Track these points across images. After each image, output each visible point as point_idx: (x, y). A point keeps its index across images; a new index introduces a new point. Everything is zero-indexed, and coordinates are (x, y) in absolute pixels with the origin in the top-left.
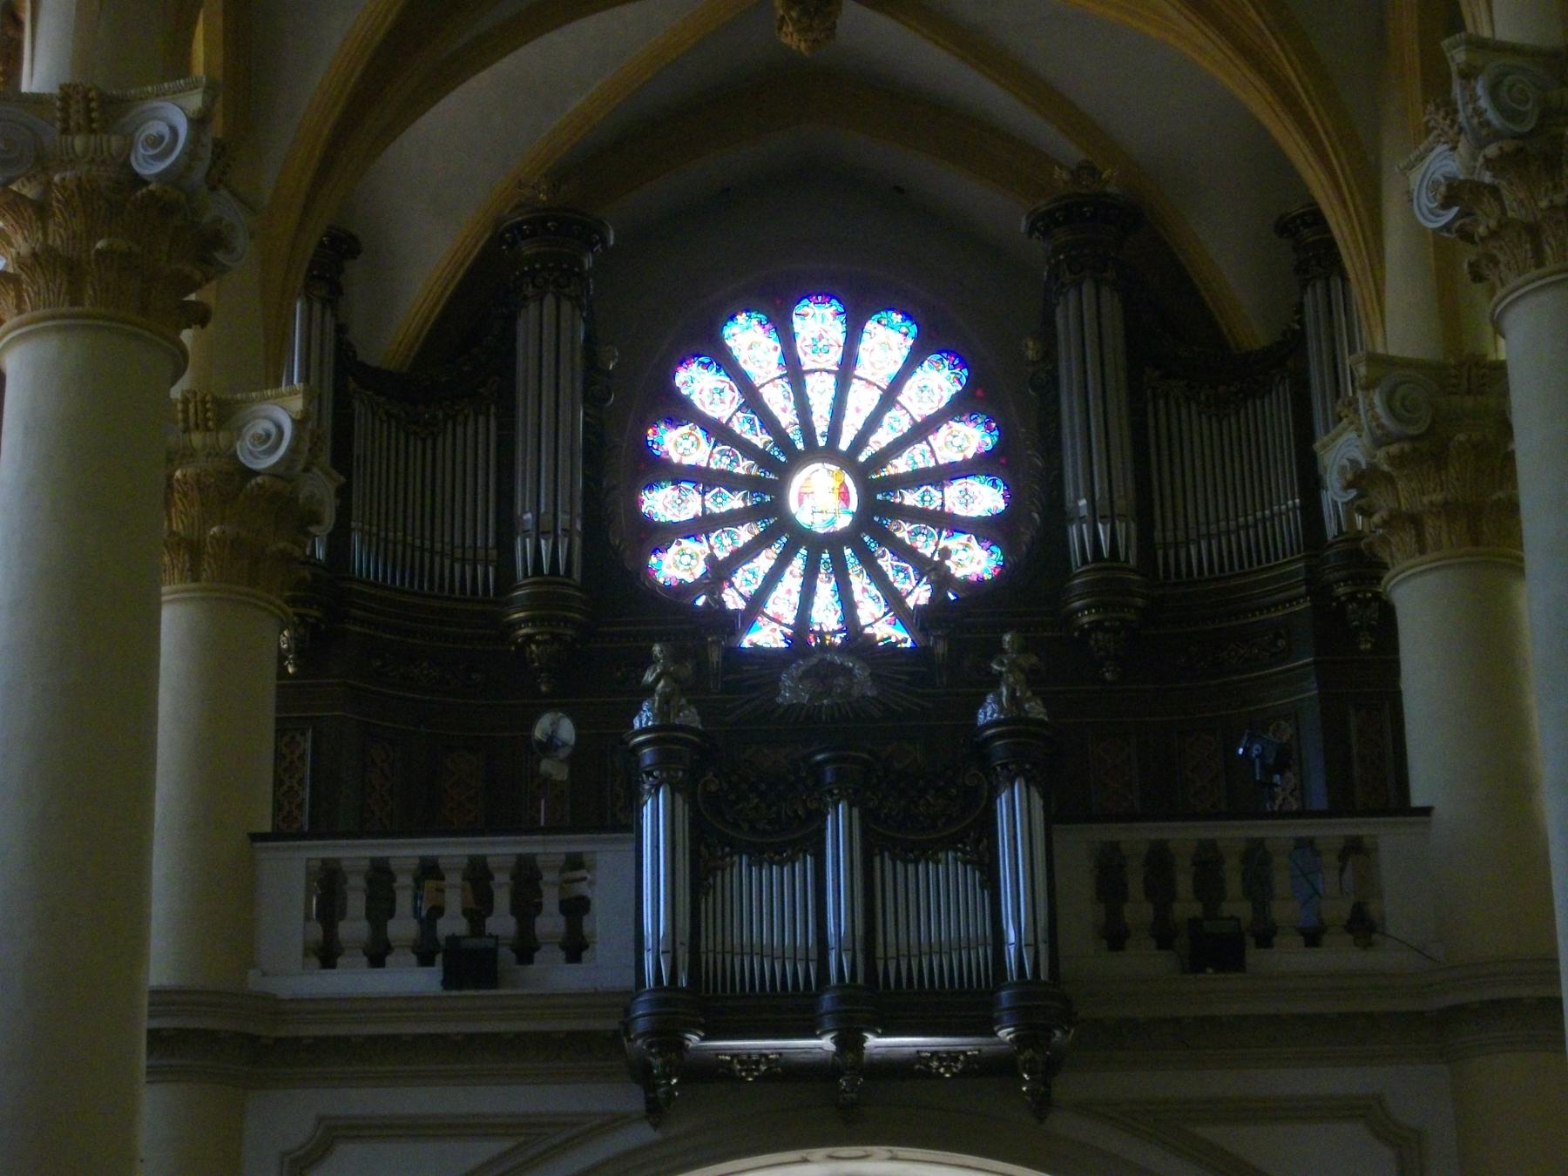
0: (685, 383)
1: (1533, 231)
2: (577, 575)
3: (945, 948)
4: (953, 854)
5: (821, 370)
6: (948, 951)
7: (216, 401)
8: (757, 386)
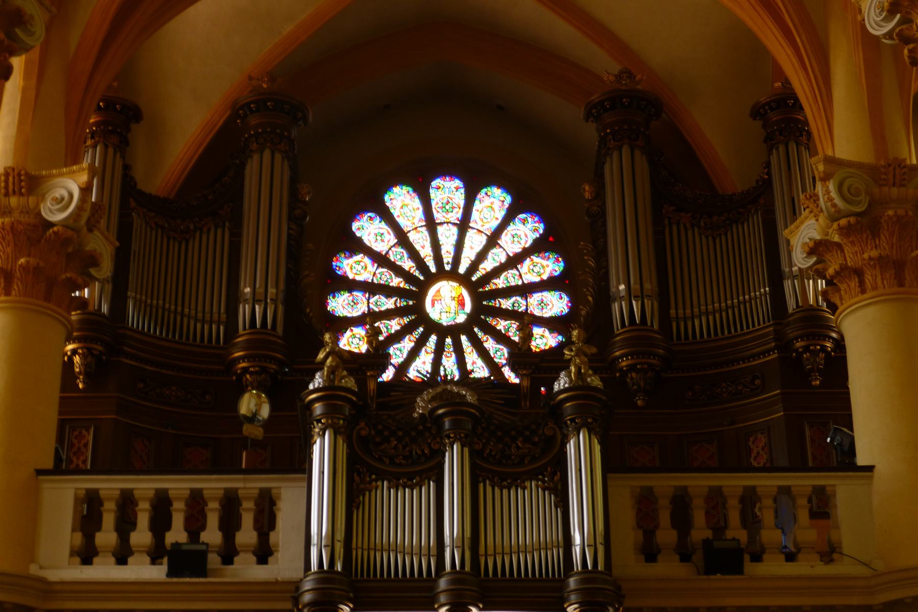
0: (359, 229)
2: (280, 330)
4: (536, 482)
5: (448, 223)
6: (531, 550)
7: (27, 174)
8: (406, 232)
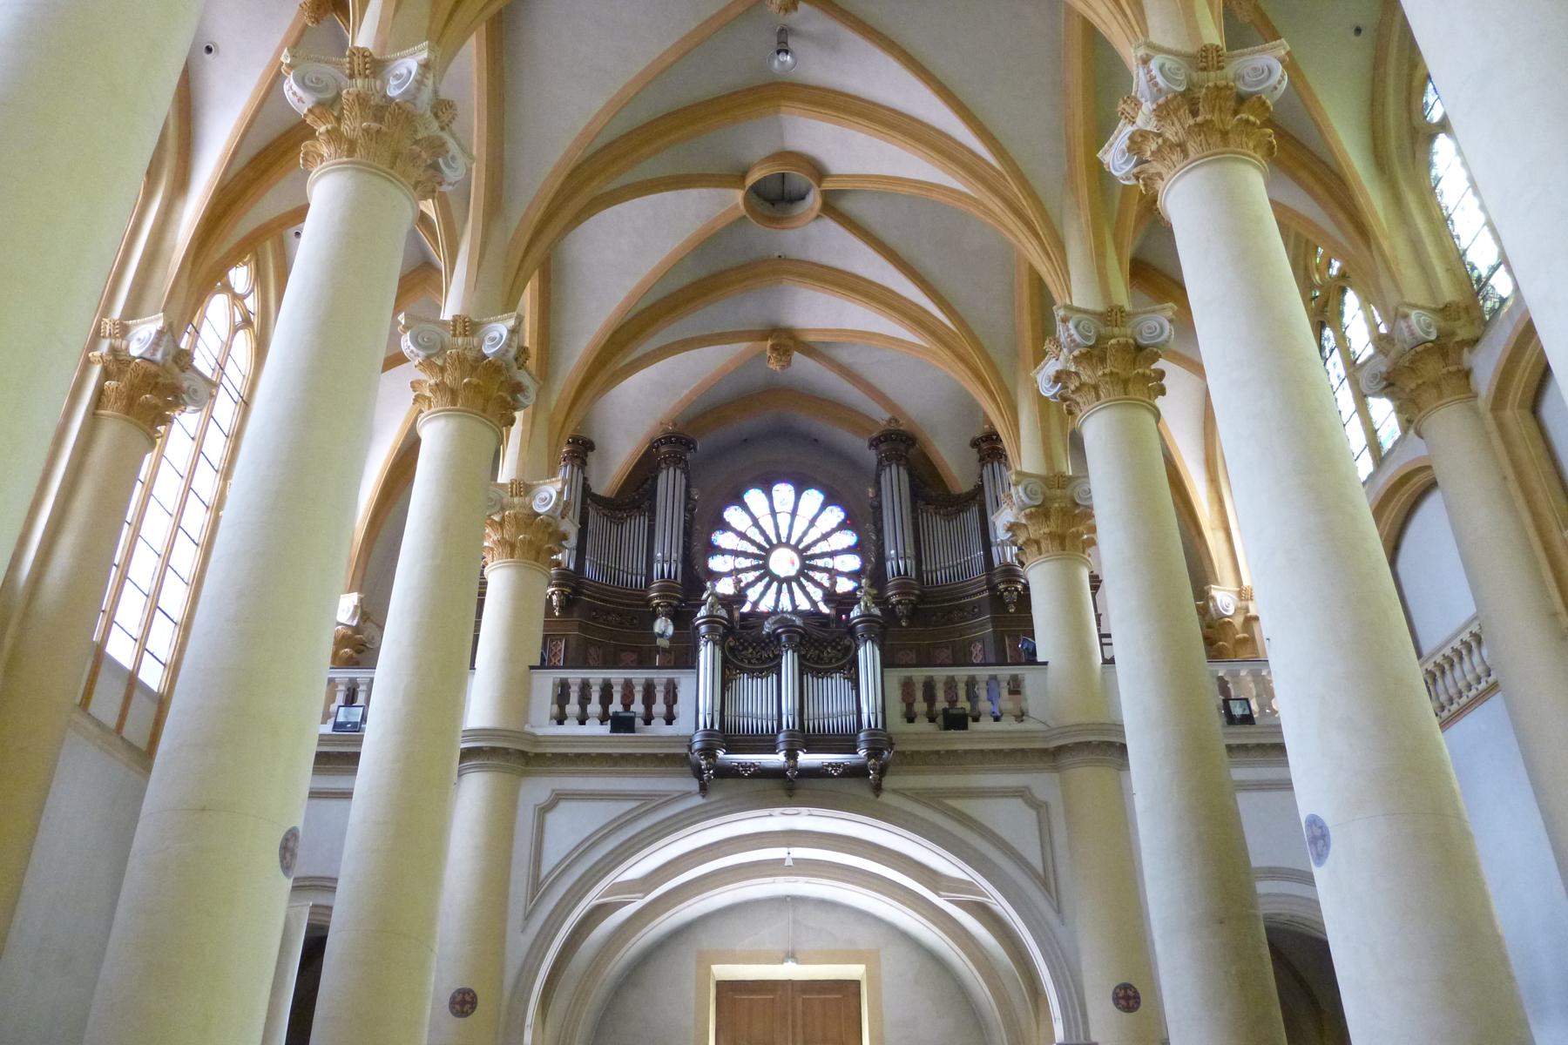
1: (1096, 388)
3: (835, 715)
